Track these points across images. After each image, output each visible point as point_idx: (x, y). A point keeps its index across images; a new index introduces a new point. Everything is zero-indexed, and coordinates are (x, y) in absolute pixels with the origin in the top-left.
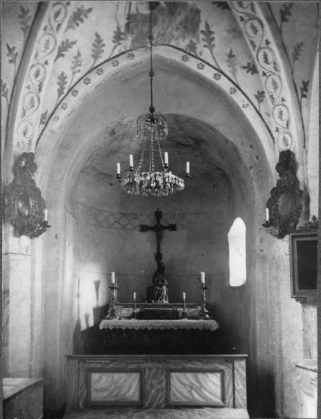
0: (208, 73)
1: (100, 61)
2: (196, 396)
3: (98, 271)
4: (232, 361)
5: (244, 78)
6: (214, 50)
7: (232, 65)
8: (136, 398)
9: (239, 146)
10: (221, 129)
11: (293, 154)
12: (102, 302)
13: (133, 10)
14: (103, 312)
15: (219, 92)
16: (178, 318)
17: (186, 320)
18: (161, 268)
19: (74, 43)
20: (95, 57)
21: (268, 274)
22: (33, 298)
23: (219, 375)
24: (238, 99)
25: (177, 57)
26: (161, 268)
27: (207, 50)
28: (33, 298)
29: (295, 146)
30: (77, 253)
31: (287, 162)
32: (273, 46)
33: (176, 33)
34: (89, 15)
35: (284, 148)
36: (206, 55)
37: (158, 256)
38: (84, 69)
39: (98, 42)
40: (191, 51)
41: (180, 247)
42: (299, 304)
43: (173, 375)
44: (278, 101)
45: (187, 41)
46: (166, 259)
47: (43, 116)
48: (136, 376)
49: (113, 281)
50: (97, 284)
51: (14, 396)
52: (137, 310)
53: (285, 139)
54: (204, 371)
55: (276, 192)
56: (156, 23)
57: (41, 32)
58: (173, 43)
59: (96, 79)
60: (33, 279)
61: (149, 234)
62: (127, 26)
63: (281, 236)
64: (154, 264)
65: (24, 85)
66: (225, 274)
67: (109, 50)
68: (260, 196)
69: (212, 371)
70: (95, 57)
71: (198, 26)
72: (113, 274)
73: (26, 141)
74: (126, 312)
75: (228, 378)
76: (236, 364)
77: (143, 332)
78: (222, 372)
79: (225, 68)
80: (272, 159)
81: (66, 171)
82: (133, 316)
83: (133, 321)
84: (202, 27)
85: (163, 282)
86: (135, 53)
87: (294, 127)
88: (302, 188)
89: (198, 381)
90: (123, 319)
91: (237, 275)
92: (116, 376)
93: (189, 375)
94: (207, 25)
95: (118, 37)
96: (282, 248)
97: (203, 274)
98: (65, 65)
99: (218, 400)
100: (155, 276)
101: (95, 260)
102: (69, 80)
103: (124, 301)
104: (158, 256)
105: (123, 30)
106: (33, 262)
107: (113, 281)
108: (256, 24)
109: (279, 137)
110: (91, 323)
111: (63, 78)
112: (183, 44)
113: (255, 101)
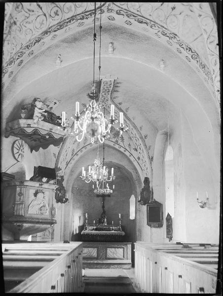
0: (122, 150)
2: (115, 255)
4: (126, 245)
5: (133, 152)
8: (96, 256)
9: (132, 173)
10: (126, 167)
11: (149, 178)
12: (81, 224)
14: (82, 228)
16: (110, 231)
17: (113, 231)
18: (104, 212)
22: (61, 223)
23: (123, 249)
24: (132, 158)
26: (104, 212)
28: (61, 223)
30: (73, 207)
31: (147, 180)
32: (142, 145)
37: (103, 207)
41: (112, 203)
42: (149, 227)
43: (108, 249)
45: (115, 140)
46: (106, 208)
48: (96, 249)
49: (87, 217)
50: (80, 218)
52: (95, 227)
54: (118, 248)
55: (143, 190)
59: (84, 150)
60: (61, 217)
61: (100, 198)
63: (145, 205)
64: (100, 198)
65: (62, 154)
66: (128, 215)
68: (139, 190)
69: (121, 248)
72: (86, 214)
74: (91, 228)
75: (125, 250)
76: (128, 245)
77: (97, 235)
78: (123, 248)
80: (143, 180)
82: (93, 229)
83: (93, 231)
85: (105, 217)
87: (149, 170)
88: (151, 190)
89: (115, 251)
90: (89, 230)
91: (132, 216)
92: (90, 249)
93: (113, 249)
96: (144, 208)
99: (122, 257)
100: (102, 214)
101: (79, 208)
103: (90, 224)
104: (103, 207)
106: (62, 211)
107: (87, 217)
110: (77, 232)
111: (73, 150)
113: (137, 159)
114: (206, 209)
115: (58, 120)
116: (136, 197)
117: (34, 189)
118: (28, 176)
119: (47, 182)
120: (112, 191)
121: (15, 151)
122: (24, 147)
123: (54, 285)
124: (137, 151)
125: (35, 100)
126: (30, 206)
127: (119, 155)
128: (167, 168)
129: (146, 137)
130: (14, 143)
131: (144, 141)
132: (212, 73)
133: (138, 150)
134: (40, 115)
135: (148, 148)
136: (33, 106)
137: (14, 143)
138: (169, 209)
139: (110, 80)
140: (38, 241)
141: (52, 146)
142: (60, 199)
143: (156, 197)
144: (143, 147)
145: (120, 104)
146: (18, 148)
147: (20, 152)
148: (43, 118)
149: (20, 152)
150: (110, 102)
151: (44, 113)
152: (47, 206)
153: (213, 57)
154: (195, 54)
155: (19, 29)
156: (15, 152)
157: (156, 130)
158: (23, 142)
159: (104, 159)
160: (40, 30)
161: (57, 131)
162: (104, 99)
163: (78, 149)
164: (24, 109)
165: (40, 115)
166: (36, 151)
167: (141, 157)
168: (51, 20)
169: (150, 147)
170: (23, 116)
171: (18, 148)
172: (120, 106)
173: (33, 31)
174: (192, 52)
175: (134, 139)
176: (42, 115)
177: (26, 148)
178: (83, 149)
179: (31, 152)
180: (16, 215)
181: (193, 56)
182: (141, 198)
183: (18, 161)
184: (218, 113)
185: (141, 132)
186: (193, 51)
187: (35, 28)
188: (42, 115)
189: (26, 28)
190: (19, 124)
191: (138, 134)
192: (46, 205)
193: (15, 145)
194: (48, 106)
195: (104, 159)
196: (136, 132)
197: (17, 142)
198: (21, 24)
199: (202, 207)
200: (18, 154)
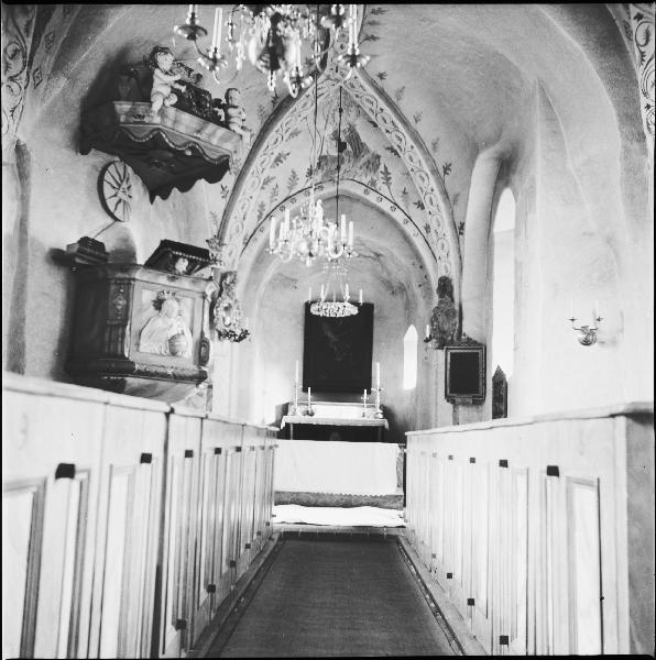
0: (385, 206)
1: (294, 192)
3: (59, 279)
5: (414, 211)
6: (392, 187)
11: (450, 281)
13: (324, 153)
15: (393, 222)
19: (273, 178)
20: (290, 188)
21: (202, 589)
24: (409, 229)
25: (359, 191)
27: (385, 187)
29: (453, 275)
31: (445, 287)
32: (437, 191)
33: (359, 171)
34: (288, 157)
35: (444, 274)
36: (384, 190)
39: (294, 175)
40: (371, 187)
42: (450, 406)
44: (441, 236)
45: (369, 178)
53: (446, 267)
56: (343, 162)
57: (249, 175)
62: (319, 164)
70: (290, 188)
71: (378, 166)
73: (231, 261)
79: (399, 201)
84: (382, 168)
86: (324, 185)
87: (453, 258)
94: (386, 168)
95: (310, 173)
96: (440, 358)
97: (361, 292)
105: (315, 167)
108: (424, 175)
111: (262, 206)
113: (424, 232)
114: (595, 346)
115: (216, 109)
116: (421, 331)
117: (153, 290)
118: (141, 259)
119: (189, 272)
121: (108, 192)
122: (132, 182)
123: (144, 465)
124: (423, 208)
125: (158, 50)
126: (144, 333)
127: (379, 223)
128: (497, 250)
129: (447, 169)
130: (105, 169)
131: (441, 182)
133: (427, 203)
134: (166, 91)
135: (451, 197)
136: (150, 63)
137: (105, 169)
138: (499, 359)
141: (202, 184)
142: (224, 319)
143: (470, 329)
144: (438, 198)
145: (381, 76)
146: (115, 185)
147: (120, 195)
148: (174, 99)
149: (120, 195)
151: (177, 86)
157: (474, 151)
158: (129, 170)
161: (214, 140)
163: (276, 203)
164: (131, 75)
165: (170, 90)
166: (165, 197)
167: (433, 226)
169: (457, 196)
170: (123, 90)
171: (115, 185)
175: (416, 177)
176: (174, 91)
177: (137, 189)
179: (152, 200)
182: (433, 330)
183: (116, 219)
184: (648, 479)
185: (436, 156)
188: (174, 91)
190: (114, 115)
191: (427, 160)
193: (107, 177)
194: (191, 70)
197: (111, 169)
199: (586, 343)
200: (116, 200)
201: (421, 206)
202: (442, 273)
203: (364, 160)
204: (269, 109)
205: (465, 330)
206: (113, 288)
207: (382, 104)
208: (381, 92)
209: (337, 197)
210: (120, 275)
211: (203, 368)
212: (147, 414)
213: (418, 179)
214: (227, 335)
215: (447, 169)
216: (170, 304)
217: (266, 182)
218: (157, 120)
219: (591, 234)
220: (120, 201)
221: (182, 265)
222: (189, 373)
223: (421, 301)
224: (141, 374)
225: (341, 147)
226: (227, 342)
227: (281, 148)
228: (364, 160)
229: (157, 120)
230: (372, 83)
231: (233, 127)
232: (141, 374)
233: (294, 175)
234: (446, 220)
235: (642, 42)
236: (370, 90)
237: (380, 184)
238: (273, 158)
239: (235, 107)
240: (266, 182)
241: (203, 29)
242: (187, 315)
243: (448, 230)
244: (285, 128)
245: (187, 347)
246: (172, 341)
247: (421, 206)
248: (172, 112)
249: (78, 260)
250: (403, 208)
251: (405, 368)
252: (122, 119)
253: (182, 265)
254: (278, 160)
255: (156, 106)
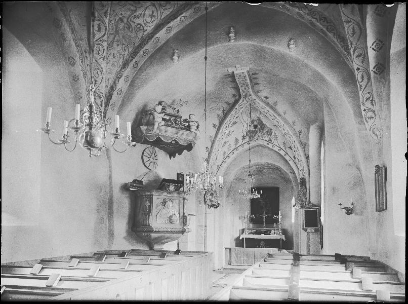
0: (276, 149)
5: (288, 151)
7: (285, 146)
11: (305, 179)
24: (287, 158)
25: (265, 143)
29: (306, 176)
32: (297, 142)
38: (232, 148)
39: (237, 140)
47: (218, 166)
51: (6, 266)
58: (263, 139)
62: (247, 134)
67: (240, 142)
70: (236, 145)
79: (282, 147)
81: (120, 58)
84: (273, 134)
87: (306, 169)
95: (244, 138)
96: (302, 212)
98: (225, 149)
102: (227, 153)
108: (290, 136)
109: (301, 173)
111: (224, 152)
112: (267, 139)
113: (293, 159)
120: (259, 196)
121: (146, 159)
127: (275, 156)
129: (300, 132)
130: (144, 150)
132: (350, 46)
133: (293, 148)
139: (242, 71)
140: (189, 250)
150: (254, 97)
152: (177, 215)
153: (350, 24)
154: (332, 24)
155: (128, 27)
156: (145, 161)
159: (250, 161)
160: (152, 24)
162: (246, 94)
167: (296, 157)
168: (162, 10)
172: (267, 101)
173: (144, 26)
174: (327, 23)
178: (235, 151)
179: (170, 158)
180: (144, 225)
181: (329, 27)
185: (295, 127)
186: (328, 21)
187: (145, 22)
189: (136, 24)
192: (176, 214)
193: (145, 154)
195: (250, 161)
196: (288, 128)
198: (129, 20)
200: (150, 162)
201: (290, 148)
202: (301, 176)
203: (265, 131)
204: (222, 115)
205: (312, 200)
206: (145, 199)
207: (268, 109)
208: (268, 104)
209: (250, 149)
210: (147, 193)
211: (185, 227)
212: (311, 190)
213: (288, 138)
214: (211, 206)
215: (300, 132)
216: (169, 204)
217: (225, 143)
218: (158, 131)
219: (350, 165)
220: (151, 163)
221: (172, 188)
222: (178, 230)
223: (295, 188)
224: (156, 232)
225: (256, 127)
226: (212, 208)
227: (230, 129)
228: (265, 131)
229: (158, 131)
230: (262, 101)
231: (192, 130)
232: (156, 232)
233: (237, 140)
234: (302, 154)
235: (360, 80)
236: (262, 104)
237: (273, 140)
238: (226, 134)
239: (192, 122)
240: (225, 143)
241: (87, 136)
242: (177, 207)
243: (303, 159)
244: (229, 122)
245: (177, 219)
246: (170, 217)
247: (290, 148)
248: (163, 128)
249: (131, 189)
250: (284, 149)
251: (291, 215)
252: (144, 132)
253: (172, 188)
254: (229, 134)
255: (156, 127)
